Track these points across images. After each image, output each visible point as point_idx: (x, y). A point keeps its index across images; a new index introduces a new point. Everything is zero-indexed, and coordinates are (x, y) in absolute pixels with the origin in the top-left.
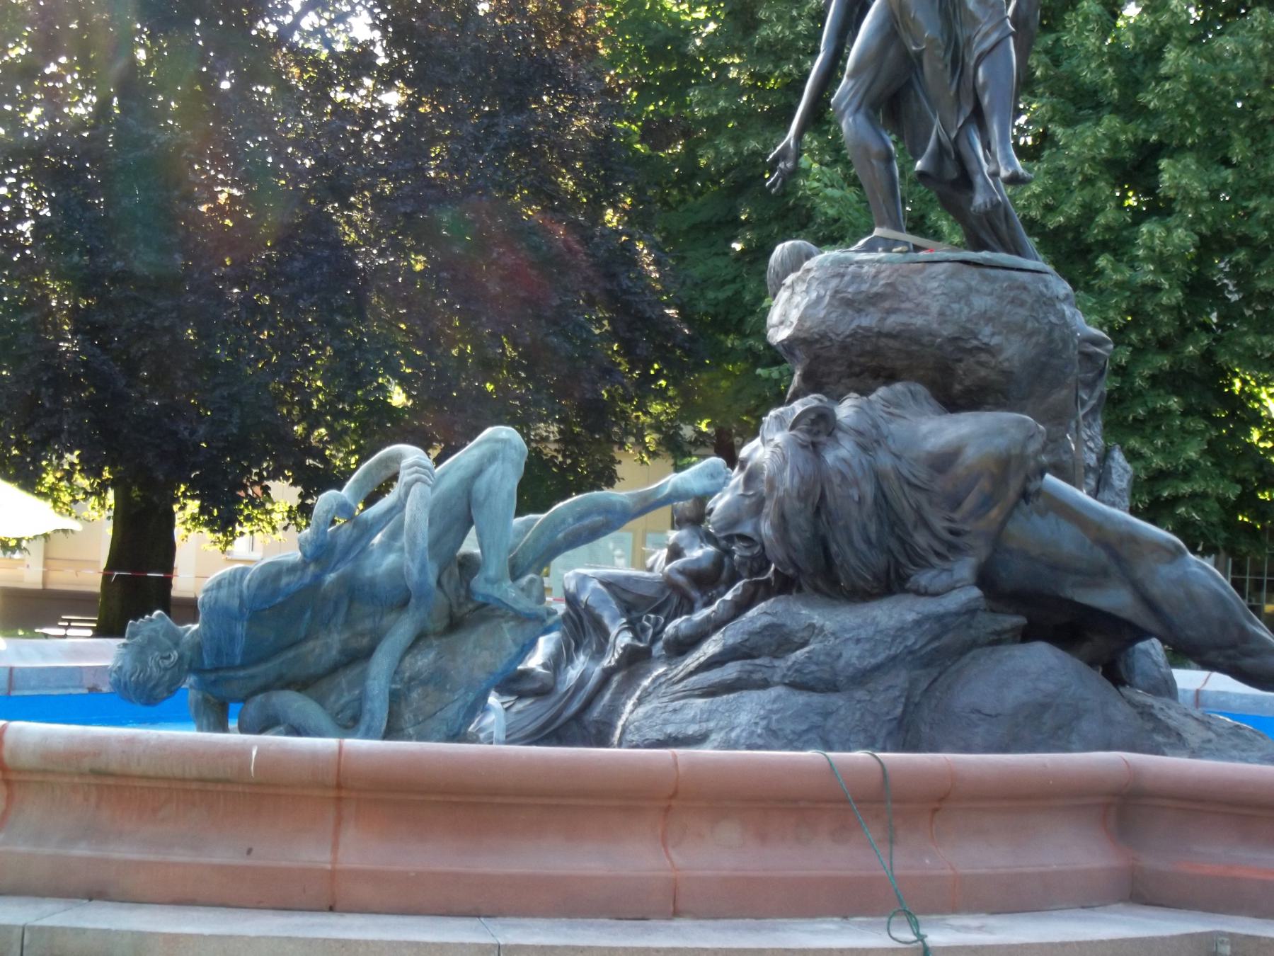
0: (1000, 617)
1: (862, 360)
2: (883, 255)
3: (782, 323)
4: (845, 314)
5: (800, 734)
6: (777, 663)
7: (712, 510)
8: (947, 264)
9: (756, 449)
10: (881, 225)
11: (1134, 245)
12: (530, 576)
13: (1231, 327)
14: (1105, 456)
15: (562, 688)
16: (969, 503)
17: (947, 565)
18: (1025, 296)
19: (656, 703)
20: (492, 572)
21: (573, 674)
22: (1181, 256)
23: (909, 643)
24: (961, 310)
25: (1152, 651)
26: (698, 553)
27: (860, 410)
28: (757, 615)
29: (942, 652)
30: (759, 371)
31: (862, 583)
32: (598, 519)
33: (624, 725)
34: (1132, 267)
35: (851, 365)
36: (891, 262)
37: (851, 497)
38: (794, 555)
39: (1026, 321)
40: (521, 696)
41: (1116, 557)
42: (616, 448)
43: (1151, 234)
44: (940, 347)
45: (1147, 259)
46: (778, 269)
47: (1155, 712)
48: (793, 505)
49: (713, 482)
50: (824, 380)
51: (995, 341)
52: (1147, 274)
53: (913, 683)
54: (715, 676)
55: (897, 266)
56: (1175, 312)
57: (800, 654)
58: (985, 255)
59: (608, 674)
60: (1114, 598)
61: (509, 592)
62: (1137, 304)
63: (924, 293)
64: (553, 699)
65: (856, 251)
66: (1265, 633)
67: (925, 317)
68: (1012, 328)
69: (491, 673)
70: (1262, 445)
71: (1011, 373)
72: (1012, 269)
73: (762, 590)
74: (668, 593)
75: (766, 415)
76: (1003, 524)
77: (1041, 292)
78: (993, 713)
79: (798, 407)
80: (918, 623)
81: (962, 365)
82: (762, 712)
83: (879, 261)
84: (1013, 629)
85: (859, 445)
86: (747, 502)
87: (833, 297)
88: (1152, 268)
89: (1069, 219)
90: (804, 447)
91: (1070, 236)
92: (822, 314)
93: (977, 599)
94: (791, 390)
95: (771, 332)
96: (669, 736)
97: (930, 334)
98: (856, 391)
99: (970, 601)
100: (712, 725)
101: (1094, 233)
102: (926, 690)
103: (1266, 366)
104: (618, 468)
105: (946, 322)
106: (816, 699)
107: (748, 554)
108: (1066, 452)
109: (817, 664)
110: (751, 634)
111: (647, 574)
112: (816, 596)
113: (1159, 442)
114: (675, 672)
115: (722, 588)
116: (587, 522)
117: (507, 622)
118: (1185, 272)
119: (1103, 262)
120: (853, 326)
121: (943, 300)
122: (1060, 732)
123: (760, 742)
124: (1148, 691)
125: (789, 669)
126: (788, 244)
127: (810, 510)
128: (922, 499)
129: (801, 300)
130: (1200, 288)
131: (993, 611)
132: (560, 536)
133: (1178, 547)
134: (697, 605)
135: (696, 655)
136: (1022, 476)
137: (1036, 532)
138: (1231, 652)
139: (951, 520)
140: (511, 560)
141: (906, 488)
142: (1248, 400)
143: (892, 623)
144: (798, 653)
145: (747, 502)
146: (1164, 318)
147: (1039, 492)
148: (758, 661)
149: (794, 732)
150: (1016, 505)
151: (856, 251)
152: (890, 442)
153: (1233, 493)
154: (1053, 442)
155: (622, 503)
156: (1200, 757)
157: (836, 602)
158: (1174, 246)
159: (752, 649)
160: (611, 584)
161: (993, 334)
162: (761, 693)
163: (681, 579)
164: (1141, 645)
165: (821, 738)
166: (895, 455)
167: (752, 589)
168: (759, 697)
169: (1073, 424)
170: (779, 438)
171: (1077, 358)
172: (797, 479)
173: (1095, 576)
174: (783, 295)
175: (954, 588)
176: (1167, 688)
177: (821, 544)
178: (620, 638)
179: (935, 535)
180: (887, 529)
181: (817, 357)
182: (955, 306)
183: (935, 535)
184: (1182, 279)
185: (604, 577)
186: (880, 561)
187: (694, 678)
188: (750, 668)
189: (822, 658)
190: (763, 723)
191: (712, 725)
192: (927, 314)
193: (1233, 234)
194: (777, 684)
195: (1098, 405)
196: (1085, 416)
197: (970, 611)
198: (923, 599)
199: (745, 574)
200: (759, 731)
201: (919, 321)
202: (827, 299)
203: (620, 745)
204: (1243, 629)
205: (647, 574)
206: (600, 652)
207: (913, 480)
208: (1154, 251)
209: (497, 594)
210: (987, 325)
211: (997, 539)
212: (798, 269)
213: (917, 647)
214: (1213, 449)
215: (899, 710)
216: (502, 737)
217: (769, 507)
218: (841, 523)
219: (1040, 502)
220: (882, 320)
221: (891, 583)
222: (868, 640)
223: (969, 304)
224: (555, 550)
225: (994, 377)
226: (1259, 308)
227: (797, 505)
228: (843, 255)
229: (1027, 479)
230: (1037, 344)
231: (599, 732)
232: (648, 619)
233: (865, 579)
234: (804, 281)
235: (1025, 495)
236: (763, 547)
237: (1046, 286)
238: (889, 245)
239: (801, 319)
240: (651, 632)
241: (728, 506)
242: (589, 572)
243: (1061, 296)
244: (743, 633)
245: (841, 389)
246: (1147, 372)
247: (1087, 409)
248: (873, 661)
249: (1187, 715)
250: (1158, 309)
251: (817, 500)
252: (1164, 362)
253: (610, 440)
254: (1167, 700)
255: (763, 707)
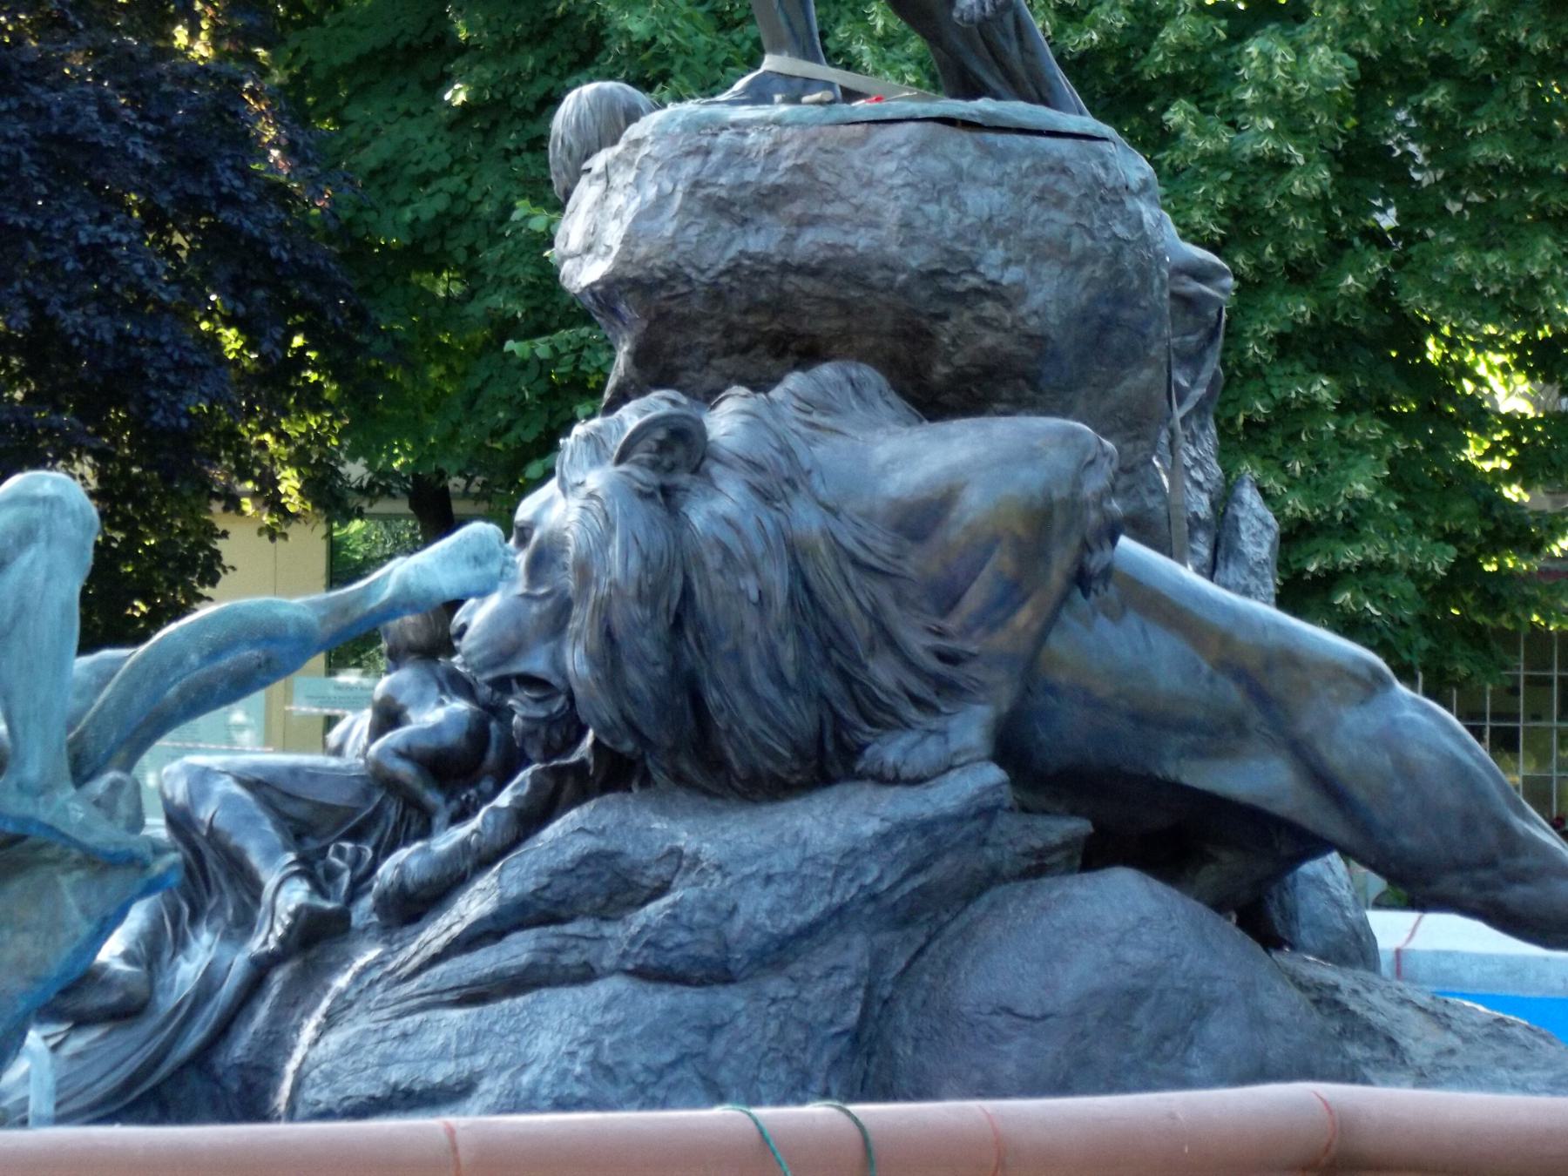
0: (1040, 822)
1: (751, 320)
2: (784, 108)
3: (589, 249)
4: (714, 228)
5: (659, 1073)
6: (608, 930)
7: (464, 628)
8: (912, 125)
9: (549, 503)
10: (777, 49)
11: (1236, 81)
12: (111, 775)
13: (1423, 237)
14: (1225, 499)
15: (166, 1003)
16: (974, 599)
17: (935, 723)
18: (1063, 186)
19: (364, 1022)
20: (32, 772)
21: (188, 971)
22: (1325, 100)
23: (869, 880)
24: (943, 217)
25: (1329, 878)
26: (436, 715)
27: (754, 419)
28: (565, 835)
29: (932, 897)
30: (510, 345)
31: (769, 764)
32: (249, 654)
33: (298, 1072)
34: (1232, 124)
35: (730, 330)
36: (801, 124)
37: (742, 593)
38: (630, 709)
39: (1068, 235)
40: (81, 1021)
41: (1260, 696)
42: (217, 507)
43: (1267, 58)
44: (904, 290)
45: (1263, 108)
46: (570, 138)
47: (1343, 997)
48: (628, 613)
49: (479, 571)
50: (678, 362)
51: (1011, 275)
52: (1261, 134)
53: (878, 959)
54: (484, 962)
55: (812, 131)
56: (1318, 211)
57: (654, 910)
58: (984, 105)
59: (261, 970)
60: (1258, 778)
61: (71, 810)
62: (1244, 196)
63: (869, 184)
64: (149, 1025)
65: (731, 103)
66: (1548, 837)
67: (876, 232)
68: (1039, 251)
69: (35, 979)
70: (1487, 466)
71: (1044, 338)
72: (1040, 133)
73: (569, 788)
74: (377, 798)
75: (568, 434)
76: (1041, 639)
77: (1095, 178)
78: (1037, 1013)
79: (631, 416)
80: (885, 839)
81: (948, 325)
82: (582, 1031)
83: (777, 122)
84: (1065, 845)
85: (754, 489)
86: (535, 609)
87: (689, 195)
88: (1271, 124)
89: (1107, 35)
90: (645, 496)
91: (1110, 66)
92: (669, 229)
93: (996, 788)
94: (612, 383)
95: (567, 268)
96: (395, 1087)
97: (884, 266)
98: (742, 381)
99: (985, 790)
100: (481, 1061)
101: (1156, 63)
102: (903, 972)
103: (1494, 311)
104: (220, 545)
105: (915, 240)
106: (692, 999)
107: (541, 713)
108: (1152, 492)
109: (691, 930)
110: (554, 873)
111: (333, 762)
112: (681, 794)
113: (1297, 467)
114: (401, 957)
115: (487, 785)
116: (226, 662)
117: (68, 871)
118: (1333, 131)
119: (1176, 115)
120: (732, 252)
121: (907, 198)
122: (1168, 1046)
123: (580, 1091)
124: (1324, 956)
125: (633, 941)
126: (588, 89)
127: (663, 624)
128: (883, 592)
129: (626, 203)
130: (1363, 163)
131: (1025, 810)
132: (172, 692)
133: (1377, 674)
134: (438, 821)
135: (444, 921)
136: (1075, 541)
137: (1107, 651)
138: (1483, 875)
139: (940, 633)
140: (71, 744)
141: (851, 573)
142: (1458, 379)
143: (833, 840)
144: (651, 908)
145: (535, 609)
146: (1298, 222)
147: (1108, 572)
148: (570, 929)
149: (647, 1069)
150: (1065, 599)
151: (731, 103)
152: (816, 480)
153: (1440, 561)
154: (1131, 472)
155: (299, 622)
156: (1436, 1084)
157: (718, 804)
158: (1310, 80)
159: (557, 904)
160: (260, 785)
161: (1007, 263)
162: (578, 992)
163: (404, 769)
164: (1309, 868)
165: (704, 1078)
166: (827, 508)
167: (550, 783)
168: (576, 1000)
169: (1164, 439)
170: (596, 479)
171: (1167, 306)
172: (634, 563)
173: (1220, 735)
174: (586, 194)
175: (951, 768)
176: (1357, 949)
177: (688, 691)
178: (283, 892)
179: (910, 664)
180: (815, 654)
181: (662, 316)
182: (932, 209)
183: (910, 664)
184: (1331, 145)
185: (245, 770)
186: (802, 718)
187: (442, 968)
188: (555, 942)
189: (698, 916)
190: (586, 1053)
191: (481, 1061)
192: (877, 226)
193: (1422, 55)
194: (611, 972)
195: (1209, 396)
196: (1183, 420)
197: (984, 812)
198: (891, 792)
199: (534, 753)
200: (578, 1069)
201: (862, 240)
202: (678, 199)
203: (291, 1115)
204: (1505, 829)
205: (333, 762)
206: (244, 924)
207: (862, 554)
208: (1274, 91)
209: (45, 816)
210: (993, 244)
211: (1030, 670)
212: (615, 142)
213: (884, 886)
214: (1399, 479)
215: (852, 1016)
216: (48, 1109)
217: (581, 619)
218: (726, 646)
219: (1112, 592)
220: (790, 238)
221: (827, 762)
222: (788, 876)
223: (959, 205)
224: (159, 722)
225: (1010, 346)
226: (1475, 198)
227: (638, 612)
228: (705, 111)
229: (1086, 547)
230: (1091, 281)
231: (248, 1087)
232: (340, 853)
233: (773, 755)
234: (630, 164)
235: (1082, 579)
236: (571, 698)
237: (1105, 166)
238: (796, 89)
239: (626, 241)
240: (346, 879)
241: (496, 619)
242: (215, 761)
243: (1134, 186)
244: (538, 874)
245: (711, 379)
246: (1268, 330)
247: (1188, 406)
248: (800, 919)
249: (1403, 1002)
250: (1285, 205)
251: (676, 603)
252: (1301, 308)
253: (205, 490)
254: (1361, 973)
255: (584, 1020)
